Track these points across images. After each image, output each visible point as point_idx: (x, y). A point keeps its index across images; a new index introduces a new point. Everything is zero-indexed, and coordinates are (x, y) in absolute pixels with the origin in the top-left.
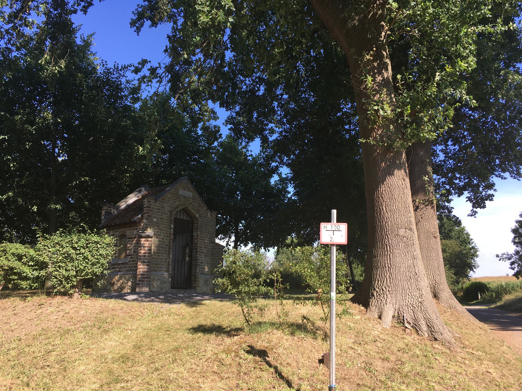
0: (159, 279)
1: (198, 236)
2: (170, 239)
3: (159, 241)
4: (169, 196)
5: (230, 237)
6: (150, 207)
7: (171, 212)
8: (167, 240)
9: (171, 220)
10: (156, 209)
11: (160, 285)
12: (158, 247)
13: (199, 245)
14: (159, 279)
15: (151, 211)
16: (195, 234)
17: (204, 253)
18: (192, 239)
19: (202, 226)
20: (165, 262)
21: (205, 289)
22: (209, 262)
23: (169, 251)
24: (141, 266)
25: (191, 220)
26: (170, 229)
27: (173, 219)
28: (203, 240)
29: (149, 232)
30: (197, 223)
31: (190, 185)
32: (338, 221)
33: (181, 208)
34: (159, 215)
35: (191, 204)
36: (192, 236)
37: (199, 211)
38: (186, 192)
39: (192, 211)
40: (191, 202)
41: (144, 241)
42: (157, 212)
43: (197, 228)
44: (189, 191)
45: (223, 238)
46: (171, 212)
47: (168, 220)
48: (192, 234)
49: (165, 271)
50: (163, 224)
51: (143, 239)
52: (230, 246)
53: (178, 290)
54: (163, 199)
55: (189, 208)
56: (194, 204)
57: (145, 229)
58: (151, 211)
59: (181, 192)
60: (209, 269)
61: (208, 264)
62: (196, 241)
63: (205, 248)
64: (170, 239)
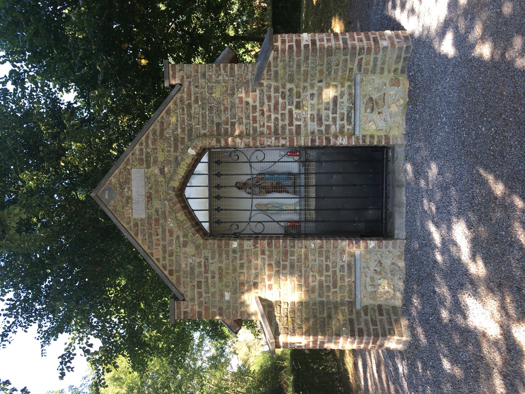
10: (200, 294)
15: (207, 309)
21: (394, 109)
37: (176, 139)
38: (134, 195)
40: (157, 171)
42: (207, 292)
44: (128, 181)
54: (171, 272)
56: (161, 158)
58: (207, 309)
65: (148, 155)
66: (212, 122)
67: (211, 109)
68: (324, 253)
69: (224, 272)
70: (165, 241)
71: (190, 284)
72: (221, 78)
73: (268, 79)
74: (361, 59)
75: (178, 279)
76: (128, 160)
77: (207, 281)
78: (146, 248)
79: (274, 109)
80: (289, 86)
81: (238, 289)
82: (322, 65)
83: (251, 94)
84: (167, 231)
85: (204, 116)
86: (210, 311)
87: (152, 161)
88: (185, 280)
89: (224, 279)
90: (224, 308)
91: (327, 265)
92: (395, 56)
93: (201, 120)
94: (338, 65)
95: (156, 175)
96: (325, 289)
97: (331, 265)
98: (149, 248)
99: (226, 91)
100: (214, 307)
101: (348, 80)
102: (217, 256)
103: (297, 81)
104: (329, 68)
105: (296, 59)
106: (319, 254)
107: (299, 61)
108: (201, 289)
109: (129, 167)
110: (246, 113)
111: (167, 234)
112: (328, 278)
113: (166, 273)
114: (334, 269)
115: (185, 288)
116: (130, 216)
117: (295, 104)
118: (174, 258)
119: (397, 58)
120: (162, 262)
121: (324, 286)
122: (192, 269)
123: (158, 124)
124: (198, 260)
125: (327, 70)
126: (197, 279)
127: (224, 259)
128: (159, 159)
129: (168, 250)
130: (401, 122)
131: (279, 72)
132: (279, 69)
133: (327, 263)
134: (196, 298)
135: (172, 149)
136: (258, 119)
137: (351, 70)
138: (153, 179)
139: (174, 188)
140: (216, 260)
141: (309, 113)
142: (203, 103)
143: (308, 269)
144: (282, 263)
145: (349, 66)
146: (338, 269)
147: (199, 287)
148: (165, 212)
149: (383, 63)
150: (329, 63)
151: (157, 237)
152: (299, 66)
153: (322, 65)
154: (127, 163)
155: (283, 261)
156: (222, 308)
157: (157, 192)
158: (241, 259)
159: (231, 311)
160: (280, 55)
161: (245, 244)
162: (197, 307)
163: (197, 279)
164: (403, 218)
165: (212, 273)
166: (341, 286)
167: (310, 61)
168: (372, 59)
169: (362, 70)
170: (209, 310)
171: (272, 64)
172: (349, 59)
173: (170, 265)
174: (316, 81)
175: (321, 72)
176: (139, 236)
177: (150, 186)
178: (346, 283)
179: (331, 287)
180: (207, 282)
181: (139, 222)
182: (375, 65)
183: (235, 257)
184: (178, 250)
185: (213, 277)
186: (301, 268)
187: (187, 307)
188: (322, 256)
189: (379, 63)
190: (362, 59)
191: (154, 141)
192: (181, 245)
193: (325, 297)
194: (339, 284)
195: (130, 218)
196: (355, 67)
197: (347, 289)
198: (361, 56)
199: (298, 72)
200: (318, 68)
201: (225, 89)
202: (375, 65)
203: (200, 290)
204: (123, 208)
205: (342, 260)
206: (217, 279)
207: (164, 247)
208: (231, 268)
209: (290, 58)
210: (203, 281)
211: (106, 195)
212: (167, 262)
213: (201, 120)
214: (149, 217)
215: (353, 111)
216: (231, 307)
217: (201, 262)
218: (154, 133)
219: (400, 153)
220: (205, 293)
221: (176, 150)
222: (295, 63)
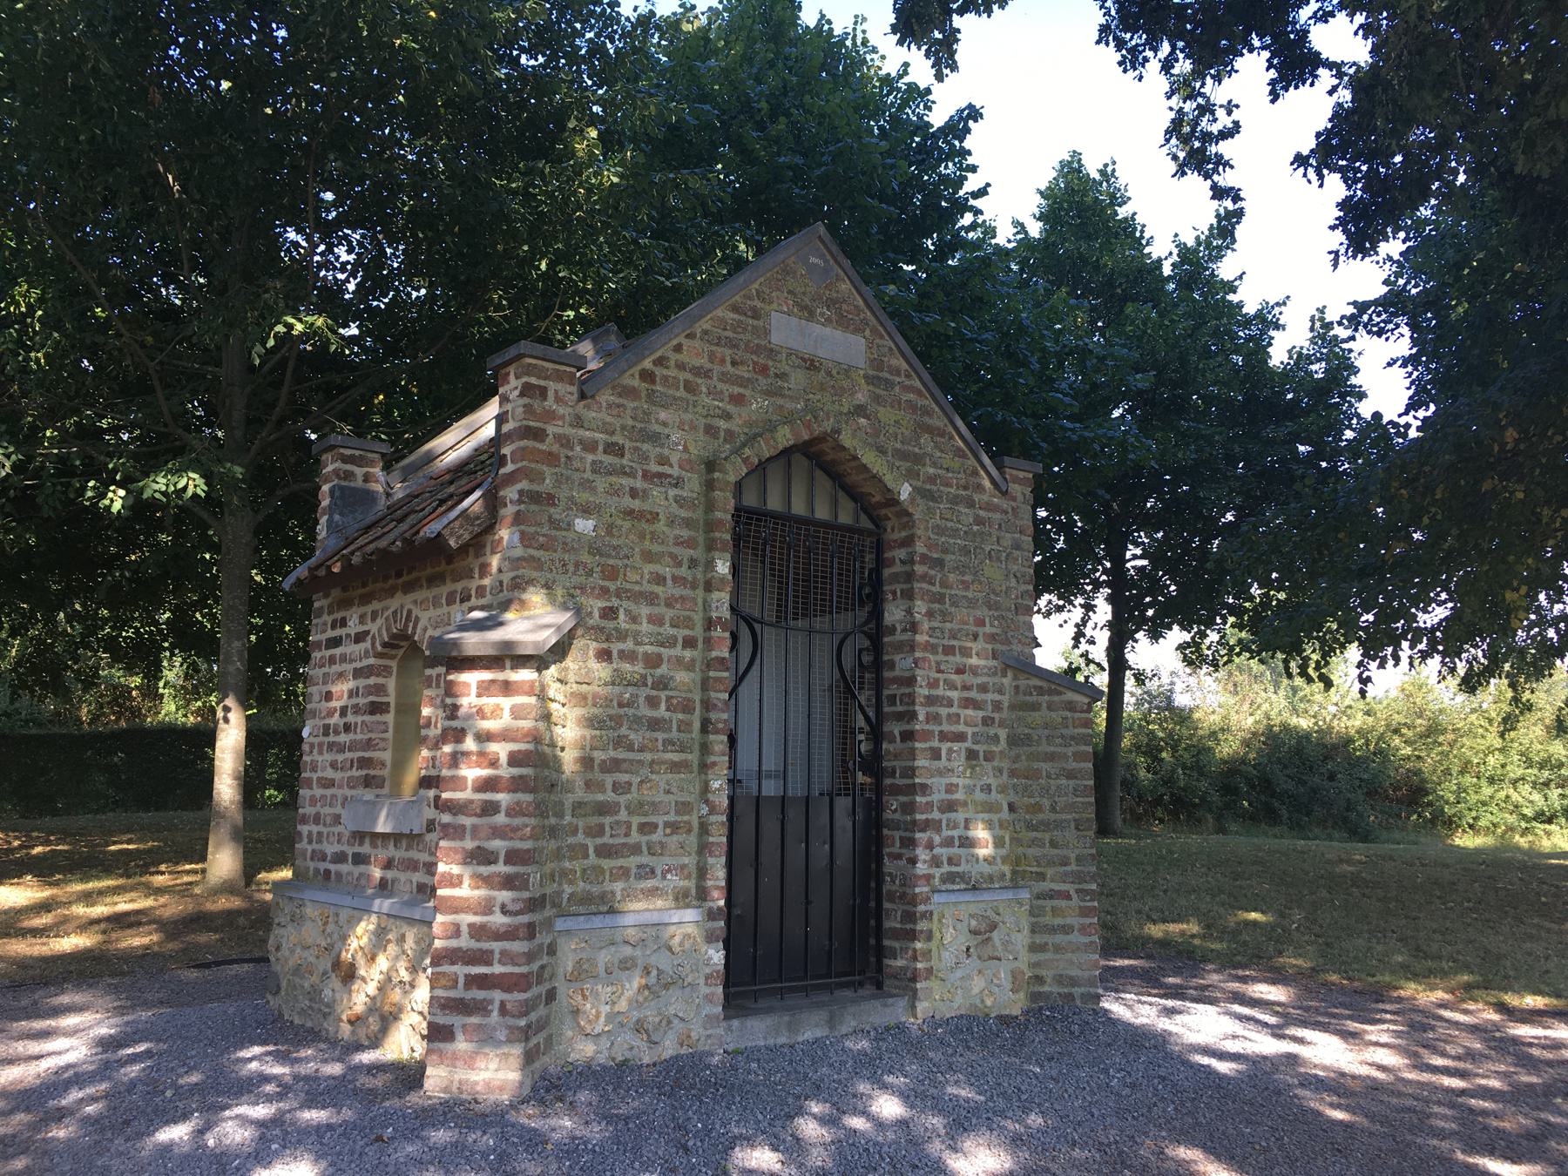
0: (626, 965)
1: (913, 627)
2: (709, 664)
3: (618, 680)
4: (695, 353)
5: (1089, 608)
6: (538, 435)
7: (711, 465)
8: (690, 667)
9: (710, 526)
10: (590, 447)
11: (635, 1004)
12: (607, 720)
13: (922, 691)
15: (551, 458)
16: (893, 614)
17: (960, 737)
18: (877, 647)
19: (940, 563)
20: (674, 827)
21: (978, 984)
22: (994, 796)
23: (705, 749)
24: (465, 891)
25: (865, 523)
26: (708, 587)
27: (724, 515)
28: (949, 651)
29: (534, 621)
30: (908, 542)
31: (845, 286)
33: (785, 437)
34: (615, 492)
35: (860, 410)
36: (876, 633)
37: (918, 459)
38: (817, 329)
39: (869, 458)
40: (861, 398)
41: (485, 689)
42: (597, 468)
43: (909, 577)
45: (1060, 609)
46: (711, 465)
47: (688, 523)
48: (877, 614)
49: (681, 899)
50: (649, 557)
51: (471, 679)
52: (1092, 642)
54: (647, 376)
55: (846, 439)
56: (886, 414)
57: (505, 600)
58: (551, 458)
59: (785, 330)
60: (998, 843)
61: (989, 808)
62: (902, 663)
63: (968, 703)
64: (709, 664)
65: (889, 385)
66: (945, 551)
67: (965, 551)
68: (686, 818)
69: (646, 526)
70: (720, 380)
71: (618, 423)
72: (1013, 582)
73: (1017, 687)
74: (1068, 897)
75: (630, 393)
76: (882, 337)
77: (625, 473)
78: (705, 324)
79: (967, 699)
80: (1003, 734)
81: (603, 560)
82: (1053, 810)
83: (989, 647)
84: (741, 390)
85: (954, 533)
86: (545, 468)
87: (878, 391)
88: (628, 412)
89: (627, 524)
90: (552, 510)
91: (656, 826)
92: (1073, 972)
93: (949, 524)
94: (1053, 844)
95: (852, 395)
96: (594, 820)
97: (655, 837)
98: (706, 332)
99: (994, 592)
100: (558, 482)
101: (1014, 872)
102: (684, 513)
103: (1012, 754)
104: (1046, 826)
105: (1070, 751)
106: (683, 803)
107: (1064, 757)
108: (605, 452)
109: (867, 332)
110: (960, 630)
111: (737, 390)
112: (622, 831)
113: (647, 364)
114: (644, 849)
115: (610, 406)
116: (775, 306)
117: (976, 747)
118: (682, 393)
119: (1071, 978)
120: (674, 357)
121: (602, 820)
122: (654, 438)
123: (941, 424)
124: (674, 459)
125: (1042, 822)
126: (628, 444)
127: (677, 532)
128: (881, 409)
129: (700, 381)
130: (956, 1005)
131: (1036, 714)
132: (1044, 712)
133: (661, 826)
134: (581, 432)
135: (898, 446)
136: (950, 658)
137: (1041, 876)
138: (845, 384)
139: (838, 432)
140: (674, 508)
141: (960, 781)
142: (974, 535)
143: (645, 771)
144: (663, 695)
145: (1050, 872)
146: (645, 859)
147: (611, 448)
148: (783, 396)
149: (1058, 949)
150: (1059, 825)
151: (728, 359)
152: (1051, 757)
153: (1053, 810)
154: (874, 331)
155: (669, 698)
156: (554, 504)
157: (822, 387)
158: (674, 578)
159: (545, 530)
160: (1077, 715)
161: (723, 594)
162: (559, 430)
163: (628, 444)
164: (765, 1038)
165: (644, 491)
166: (603, 872)
167: (1064, 782)
168: (1069, 921)
169: (1040, 902)
170: (550, 465)
171: (1056, 698)
172: (1068, 868)
173: (665, 378)
174: (1012, 797)
175: (1037, 808)
176: (732, 315)
177: (834, 372)
178: (608, 886)
179: (599, 841)
180: (623, 472)
181: (761, 323)
182: (1053, 930)
183: (680, 564)
184: (699, 409)
185: (634, 493)
186: (651, 751)
187: (558, 399)
188: (677, 813)
189: (1059, 938)
190: (1069, 897)
191: (912, 407)
192: (709, 420)
193: (575, 820)
194: (607, 864)
195: (771, 303)
196: (1046, 885)
197: (595, 889)
198: (1074, 896)
199: (1034, 757)
200: (1046, 803)
201: (998, 589)
202: (1053, 930)
203: (601, 448)
204: (790, 292)
205: (669, 871)
206: (628, 502)
207: (707, 374)
208: (656, 548)
209: (1073, 738)
210: (625, 462)
211: (809, 255)
212: (672, 373)
213: (949, 524)
214: (772, 353)
215: (963, 886)
216: (554, 533)
217: (671, 466)
218: (927, 412)
219: (892, 1012)
220: (594, 462)
221: (897, 452)
222: (1059, 749)
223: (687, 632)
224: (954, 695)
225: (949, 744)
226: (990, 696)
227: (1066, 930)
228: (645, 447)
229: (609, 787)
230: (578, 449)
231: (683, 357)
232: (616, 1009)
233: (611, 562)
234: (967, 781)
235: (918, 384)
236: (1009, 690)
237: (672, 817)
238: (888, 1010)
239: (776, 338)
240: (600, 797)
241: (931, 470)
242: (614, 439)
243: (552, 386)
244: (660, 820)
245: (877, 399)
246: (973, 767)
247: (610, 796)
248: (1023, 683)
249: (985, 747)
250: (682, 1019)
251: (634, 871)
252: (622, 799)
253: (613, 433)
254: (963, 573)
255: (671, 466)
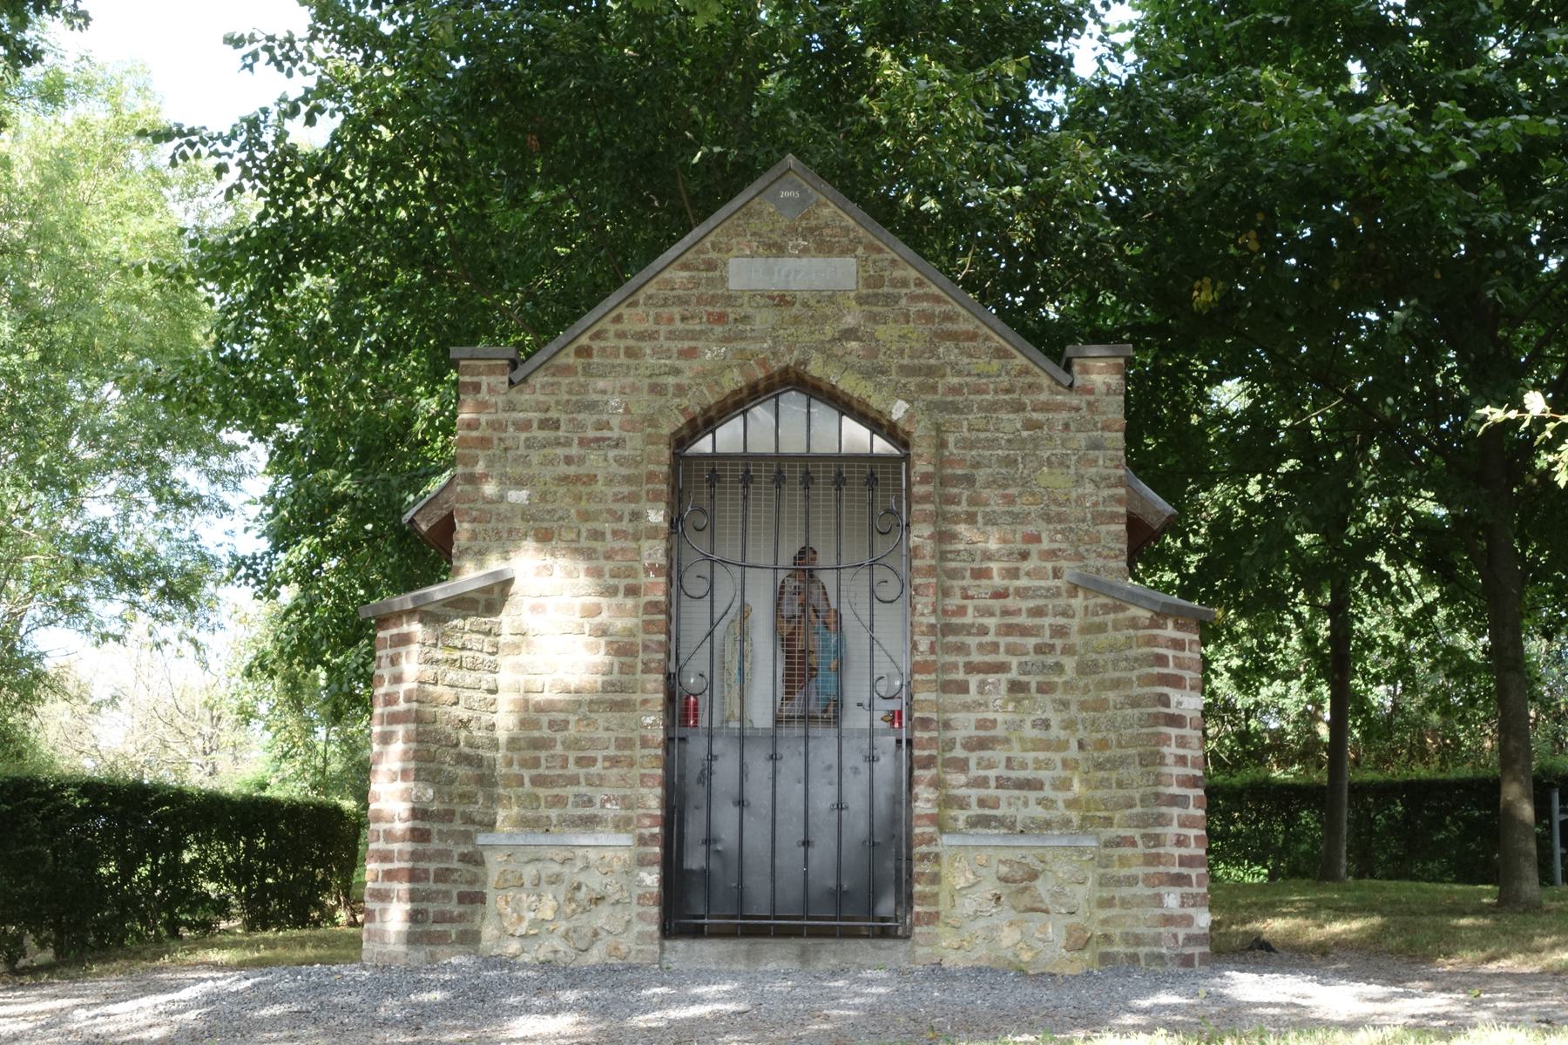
4: (636, 318)
10: (525, 426)
14: (555, 880)
32: (1359, 875)
34: (548, 462)
35: (850, 334)
37: (930, 371)
38: (788, 263)
40: (849, 321)
44: (825, 248)
53: (742, 945)
66: (977, 465)
71: (551, 400)
72: (1089, 488)
75: (568, 370)
76: (880, 251)
79: (1009, 626)
81: (537, 525)
84: (693, 344)
93: (982, 435)
94: (1120, 785)
97: (593, 770)
99: (1055, 501)
102: (624, 471)
105: (1134, 675)
106: (624, 739)
107: (1129, 682)
109: (860, 251)
111: (687, 344)
112: (558, 763)
113: (584, 340)
114: (582, 780)
115: (543, 387)
117: (1024, 678)
118: (622, 359)
119: (1136, 936)
121: (537, 753)
122: (591, 406)
123: (971, 328)
125: (1108, 760)
126: (563, 417)
127: (617, 489)
129: (643, 344)
131: (1102, 636)
135: (906, 361)
137: (1108, 822)
139: (805, 363)
141: (1000, 717)
142: (1024, 441)
145: (1117, 816)
146: (583, 789)
148: (743, 339)
149: (1124, 903)
150: (1123, 762)
151: (677, 317)
153: (1120, 745)
157: (796, 320)
158: (615, 533)
160: (1141, 632)
163: (563, 417)
167: (1129, 711)
171: (1121, 615)
172: (1134, 811)
175: (1103, 744)
177: (812, 302)
181: (717, 273)
182: (1119, 882)
183: (620, 519)
184: (642, 371)
185: (568, 460)
187: (491, 390)
188: (618, 747)
189: (1125, 891)
191: (928, 317)
192: (654, 380)
194: (542, 792)
198: (1140, 842)
199: (1102, 686)
201: (1062, 498)
202: (1119, 882)
203: (535, 425)
204: (754, 234)
205: (609, 800)
206: (563, 469)
207: (652, 336)
208: (593, 507)
209: (1136, 660)
212: (612, 342)
213: (982, 435)
214: (730, 299)
217: (611, 429)
220: (527, 439)
221: (903, 370)
223: (630, 581)
224: (991, 622)
225: (981, 676)
226: (1047, 621)
227: (1131, 881)
228: (581, 417)
229: (545, 725)
230: (511, 429)
231: (624, 326)
232: (540, 916)
233: (545, 525)
234: (1008, 717)
235: (935, 290)
236: (1080, 612)
237: (612, 752)
238: (883, 953)
239: (734, 284)
240: (536, 734)
241: (955, 380)
242: (549, 415)
243: (484, 380)
244: (599, 755)
245: (873, 318)
246: (1019, 702)
247: (546, 733)
248: (1092, 602)
249: (1040, 678)
250: (609, 933)
251: (571, 799)
252: (559, 736)
253: (547, 410)
254: (1006, 487)
255: (611, 429)
